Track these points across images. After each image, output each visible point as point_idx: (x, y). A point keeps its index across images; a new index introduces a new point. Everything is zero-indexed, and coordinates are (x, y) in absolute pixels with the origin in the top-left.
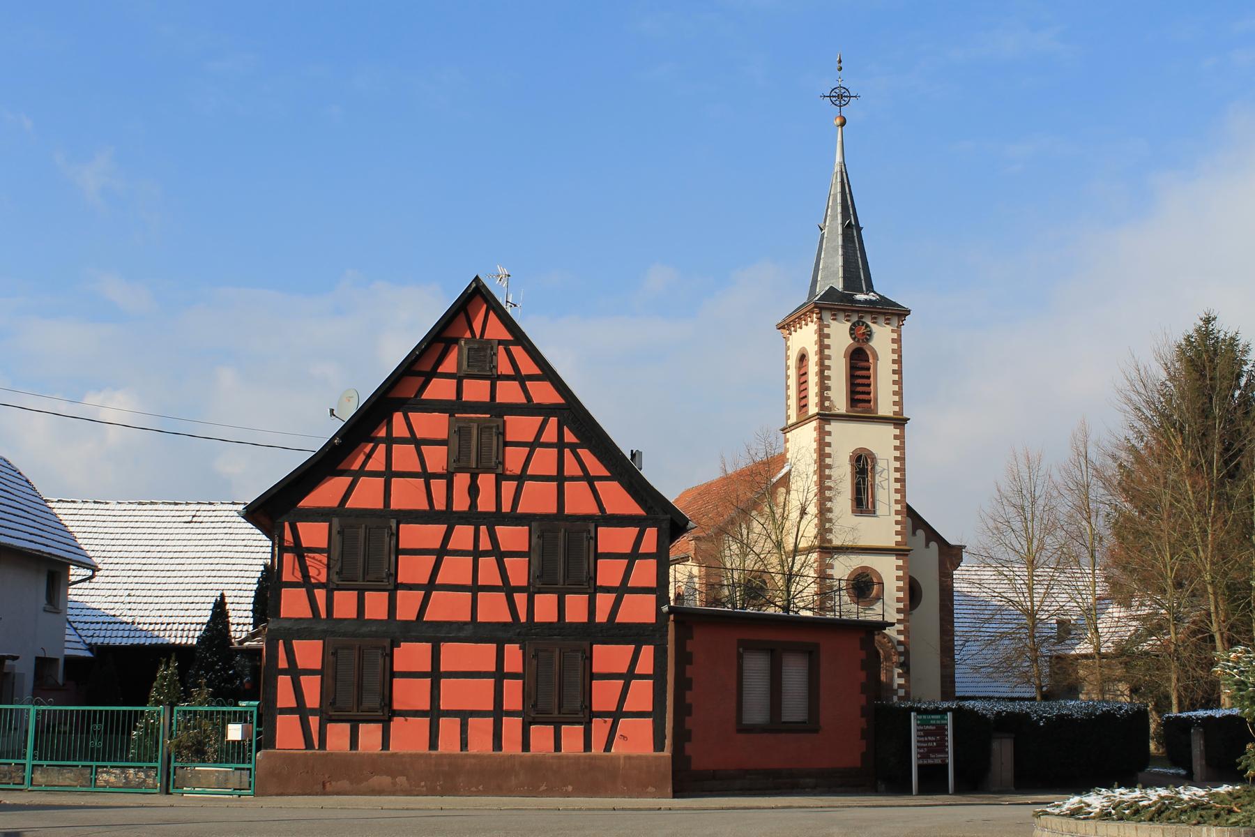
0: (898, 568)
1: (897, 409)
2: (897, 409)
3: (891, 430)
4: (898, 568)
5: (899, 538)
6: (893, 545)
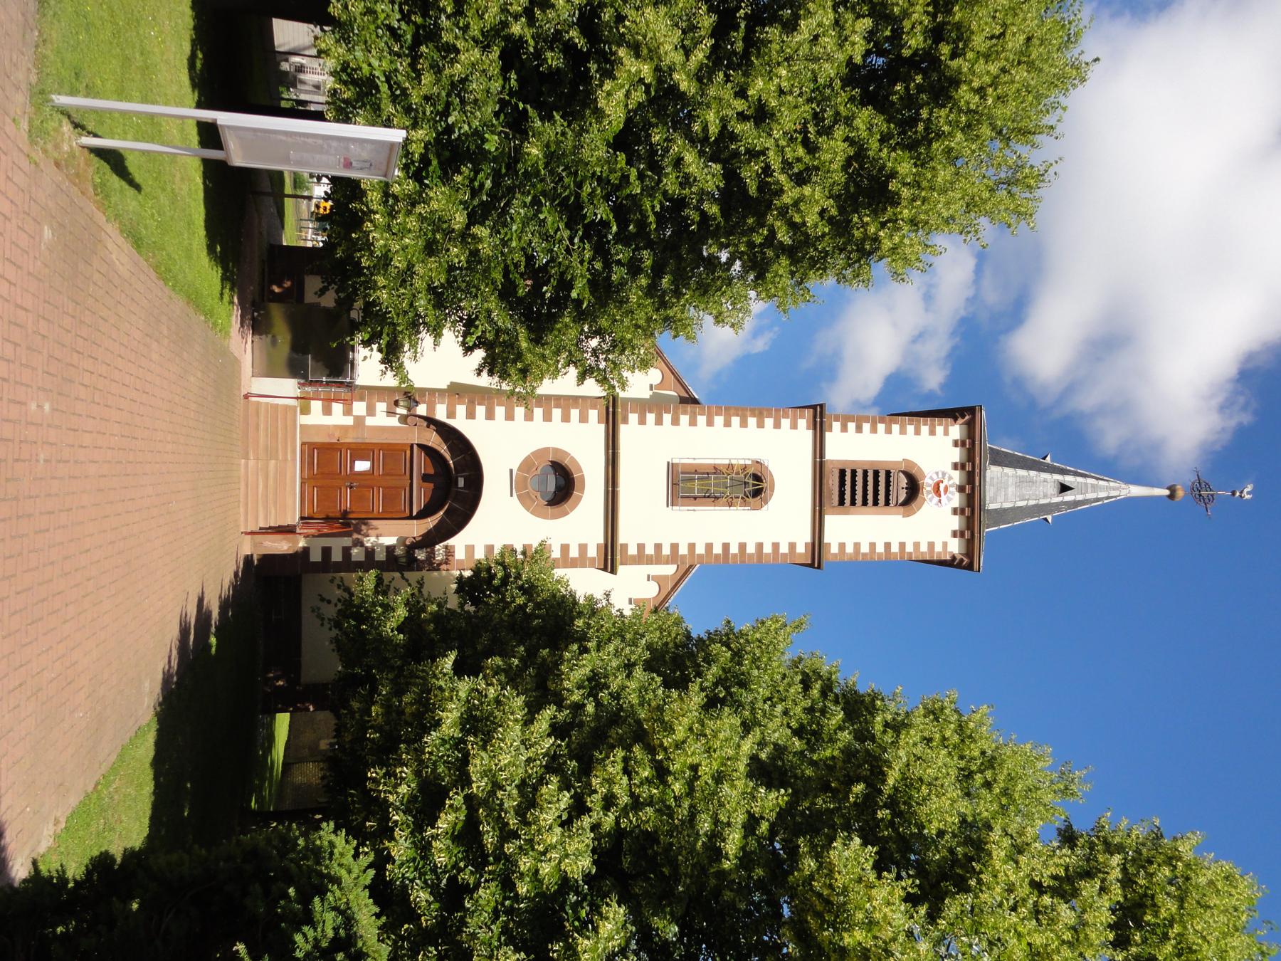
0: (792, 546)
1: (632, 551)
2: (632, 551)
3: (803, 538)
4: (792, 546)
5: (834, 549)
6: (622, 538)
